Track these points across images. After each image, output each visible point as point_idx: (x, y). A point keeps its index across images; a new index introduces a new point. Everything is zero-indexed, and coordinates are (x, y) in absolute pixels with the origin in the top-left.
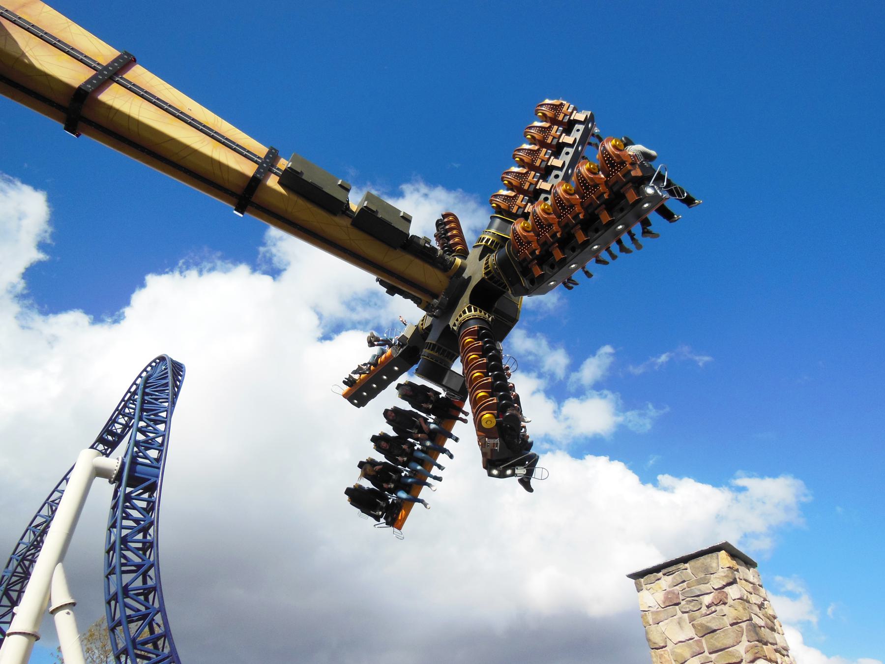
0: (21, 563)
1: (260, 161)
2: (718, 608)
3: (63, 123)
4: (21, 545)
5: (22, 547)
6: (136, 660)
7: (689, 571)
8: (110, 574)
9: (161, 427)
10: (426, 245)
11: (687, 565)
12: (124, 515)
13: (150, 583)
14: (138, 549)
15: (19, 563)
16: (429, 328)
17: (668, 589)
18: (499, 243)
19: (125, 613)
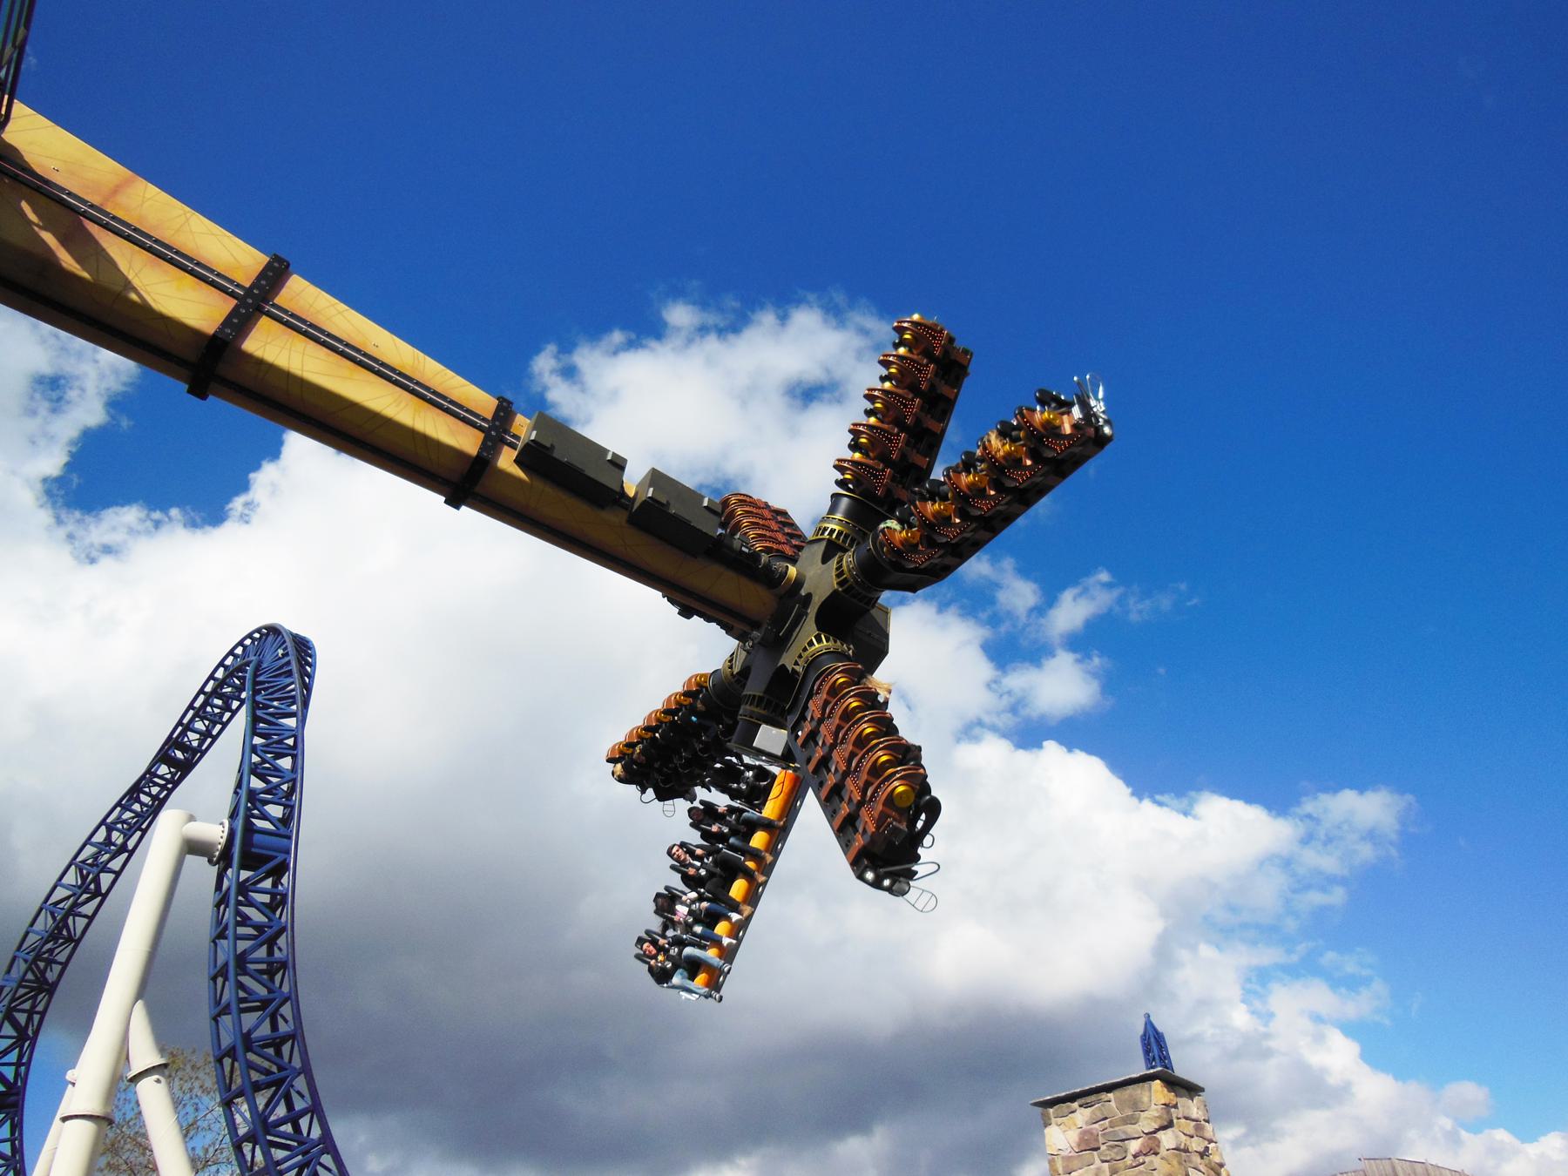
0: (33, 966)
1: (487, 426)
2: (1147, 1159)
3: (186, 382)
4: (30, 935)
5: (32, 938)
6: (270, 1151)
7: (1113, 1104)
8: (219, 1015)
9: (285, 763)
10: (744, 549)
11: (1111, 1096)
12: (239, 919)
13: (283, 1028)
14: (261, 972)
15: (31, 965)
16: (745, 672)
17: (1085, 1127)
18: (855, 540)
19: (250, 1079)
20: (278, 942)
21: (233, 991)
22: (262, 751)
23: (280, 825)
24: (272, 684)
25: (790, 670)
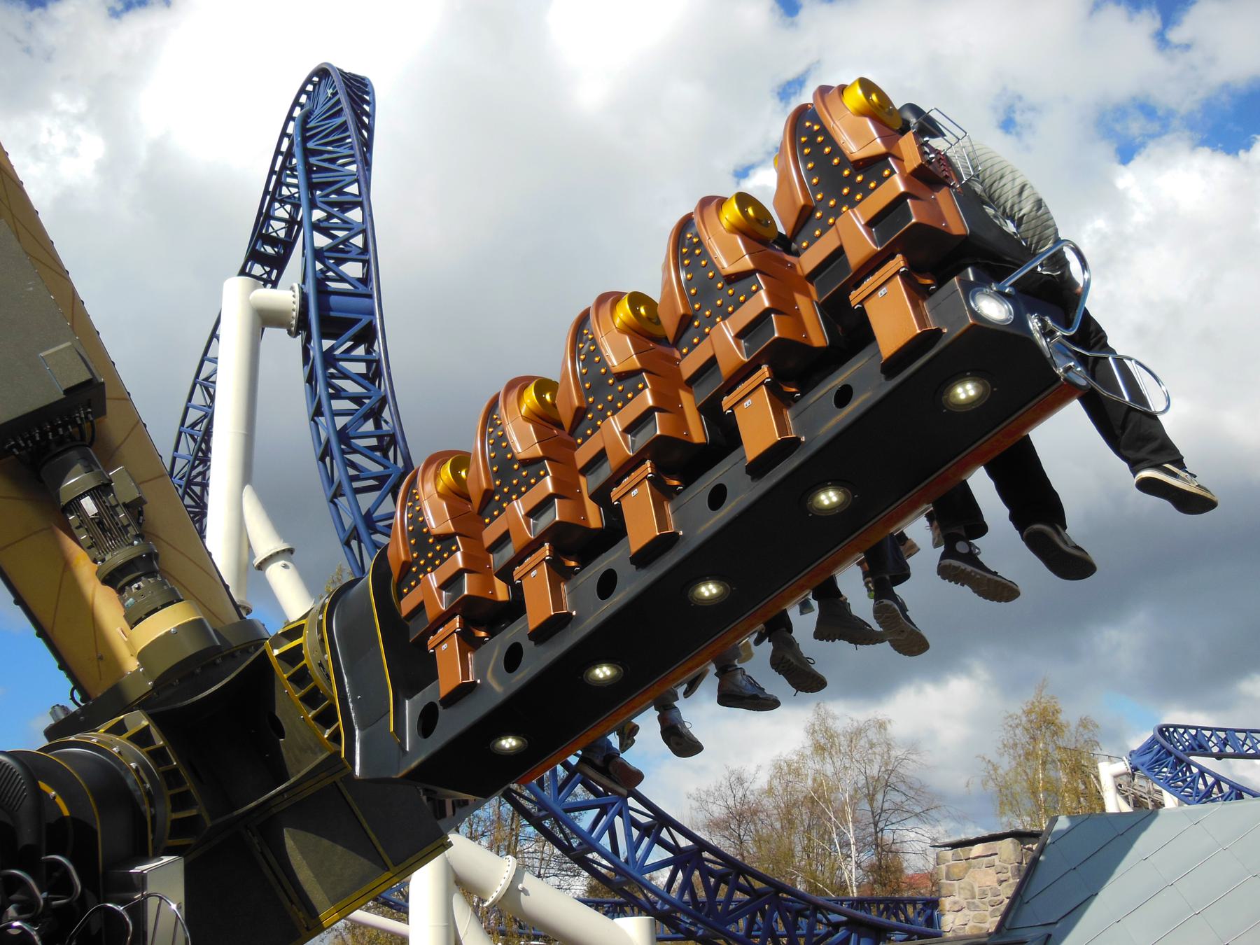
0: (188, 490)
9: (355, 215)
20: (383, 415)
21: (342, 470)
22: (322, 202)
23: (358, 284)
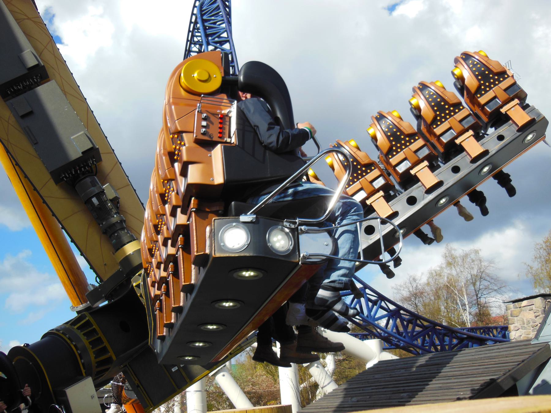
24: (210, 9)
25: (359, 251)
